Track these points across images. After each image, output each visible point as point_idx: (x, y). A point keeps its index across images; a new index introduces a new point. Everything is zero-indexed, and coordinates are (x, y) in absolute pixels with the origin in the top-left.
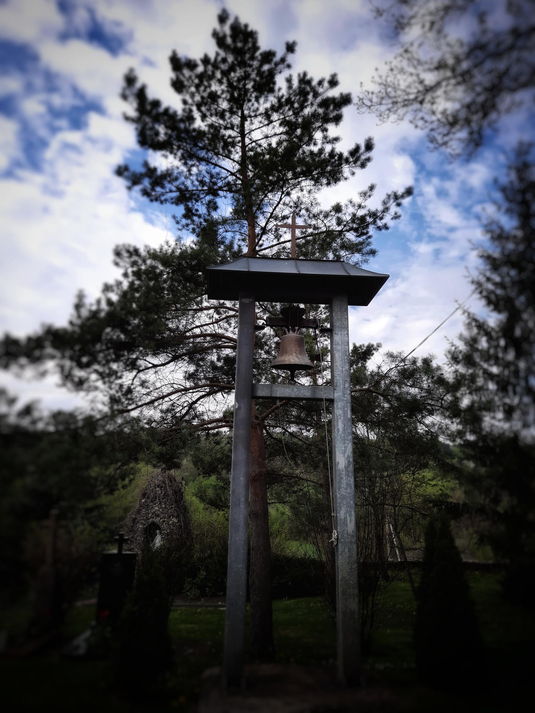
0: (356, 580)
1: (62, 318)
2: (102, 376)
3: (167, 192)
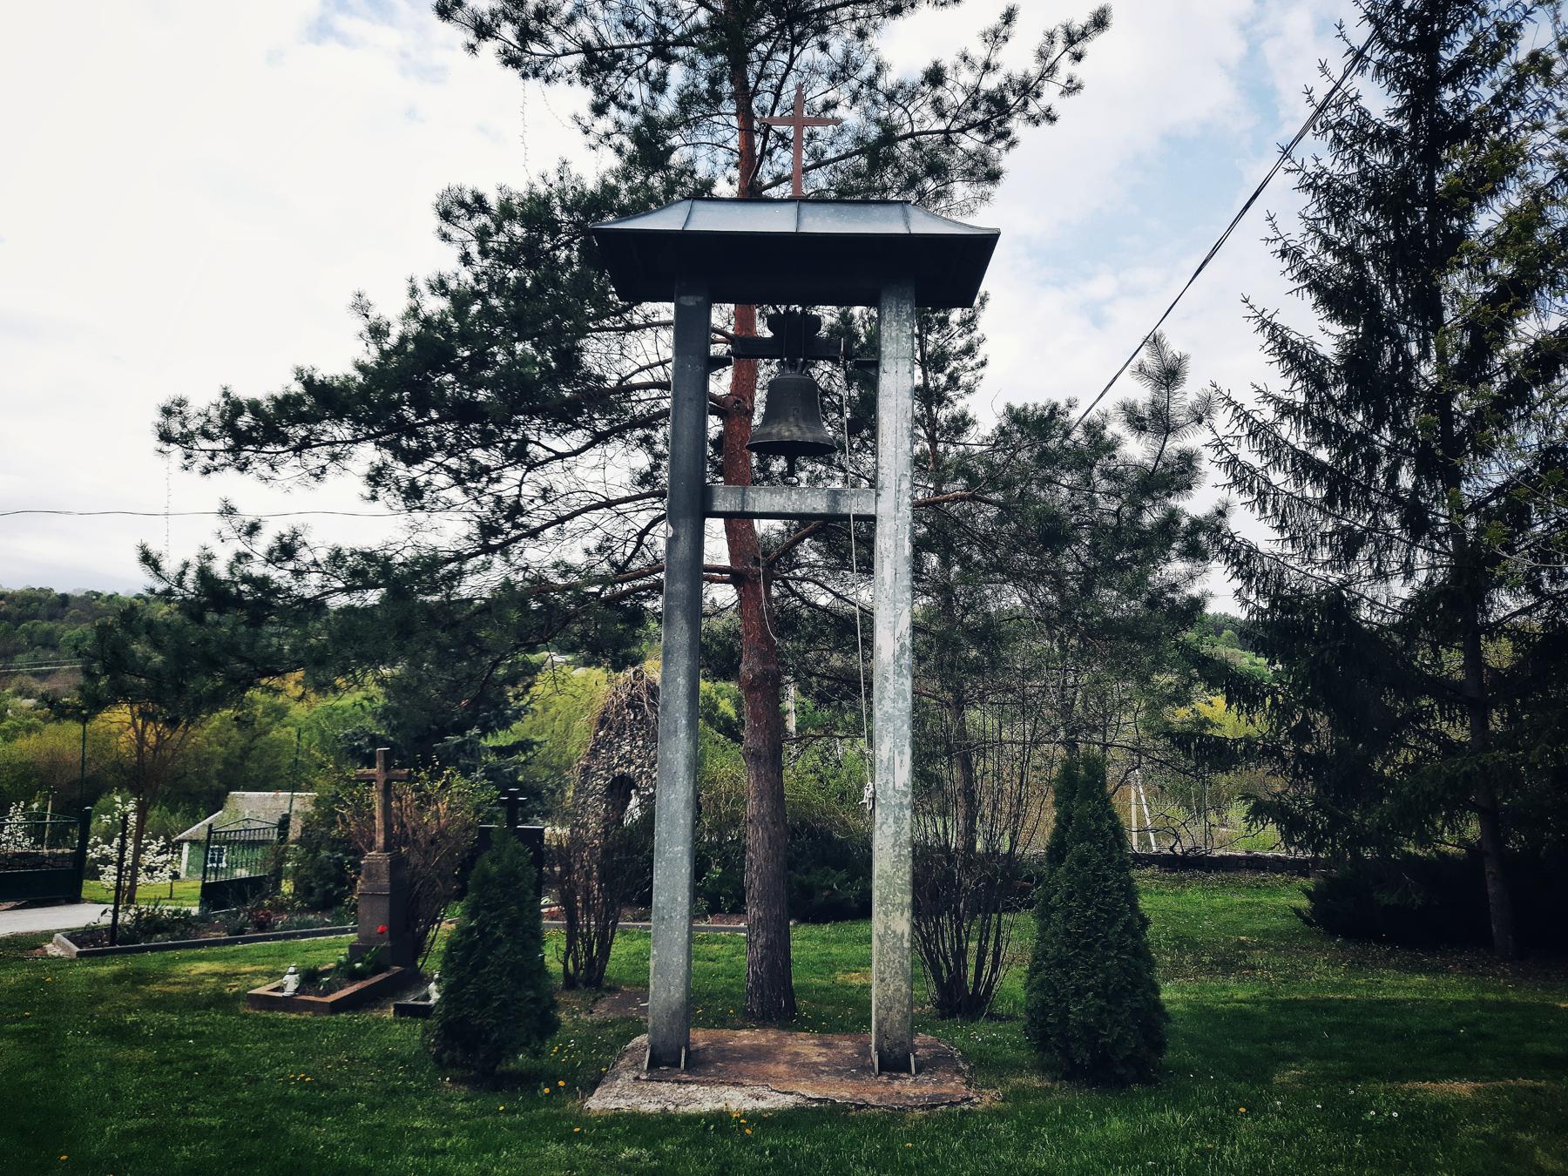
0: (908, 877)
1: (341, 356)
2: (458, 479)
3: (557, 56)
